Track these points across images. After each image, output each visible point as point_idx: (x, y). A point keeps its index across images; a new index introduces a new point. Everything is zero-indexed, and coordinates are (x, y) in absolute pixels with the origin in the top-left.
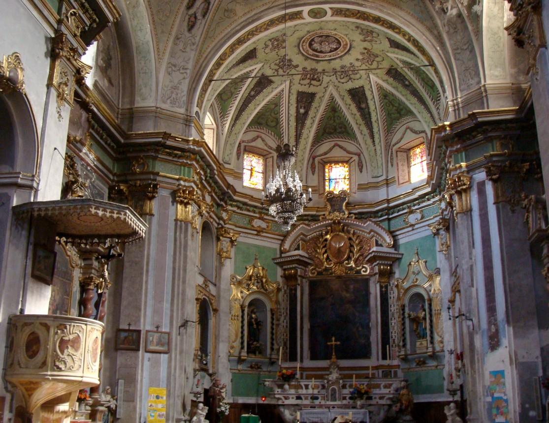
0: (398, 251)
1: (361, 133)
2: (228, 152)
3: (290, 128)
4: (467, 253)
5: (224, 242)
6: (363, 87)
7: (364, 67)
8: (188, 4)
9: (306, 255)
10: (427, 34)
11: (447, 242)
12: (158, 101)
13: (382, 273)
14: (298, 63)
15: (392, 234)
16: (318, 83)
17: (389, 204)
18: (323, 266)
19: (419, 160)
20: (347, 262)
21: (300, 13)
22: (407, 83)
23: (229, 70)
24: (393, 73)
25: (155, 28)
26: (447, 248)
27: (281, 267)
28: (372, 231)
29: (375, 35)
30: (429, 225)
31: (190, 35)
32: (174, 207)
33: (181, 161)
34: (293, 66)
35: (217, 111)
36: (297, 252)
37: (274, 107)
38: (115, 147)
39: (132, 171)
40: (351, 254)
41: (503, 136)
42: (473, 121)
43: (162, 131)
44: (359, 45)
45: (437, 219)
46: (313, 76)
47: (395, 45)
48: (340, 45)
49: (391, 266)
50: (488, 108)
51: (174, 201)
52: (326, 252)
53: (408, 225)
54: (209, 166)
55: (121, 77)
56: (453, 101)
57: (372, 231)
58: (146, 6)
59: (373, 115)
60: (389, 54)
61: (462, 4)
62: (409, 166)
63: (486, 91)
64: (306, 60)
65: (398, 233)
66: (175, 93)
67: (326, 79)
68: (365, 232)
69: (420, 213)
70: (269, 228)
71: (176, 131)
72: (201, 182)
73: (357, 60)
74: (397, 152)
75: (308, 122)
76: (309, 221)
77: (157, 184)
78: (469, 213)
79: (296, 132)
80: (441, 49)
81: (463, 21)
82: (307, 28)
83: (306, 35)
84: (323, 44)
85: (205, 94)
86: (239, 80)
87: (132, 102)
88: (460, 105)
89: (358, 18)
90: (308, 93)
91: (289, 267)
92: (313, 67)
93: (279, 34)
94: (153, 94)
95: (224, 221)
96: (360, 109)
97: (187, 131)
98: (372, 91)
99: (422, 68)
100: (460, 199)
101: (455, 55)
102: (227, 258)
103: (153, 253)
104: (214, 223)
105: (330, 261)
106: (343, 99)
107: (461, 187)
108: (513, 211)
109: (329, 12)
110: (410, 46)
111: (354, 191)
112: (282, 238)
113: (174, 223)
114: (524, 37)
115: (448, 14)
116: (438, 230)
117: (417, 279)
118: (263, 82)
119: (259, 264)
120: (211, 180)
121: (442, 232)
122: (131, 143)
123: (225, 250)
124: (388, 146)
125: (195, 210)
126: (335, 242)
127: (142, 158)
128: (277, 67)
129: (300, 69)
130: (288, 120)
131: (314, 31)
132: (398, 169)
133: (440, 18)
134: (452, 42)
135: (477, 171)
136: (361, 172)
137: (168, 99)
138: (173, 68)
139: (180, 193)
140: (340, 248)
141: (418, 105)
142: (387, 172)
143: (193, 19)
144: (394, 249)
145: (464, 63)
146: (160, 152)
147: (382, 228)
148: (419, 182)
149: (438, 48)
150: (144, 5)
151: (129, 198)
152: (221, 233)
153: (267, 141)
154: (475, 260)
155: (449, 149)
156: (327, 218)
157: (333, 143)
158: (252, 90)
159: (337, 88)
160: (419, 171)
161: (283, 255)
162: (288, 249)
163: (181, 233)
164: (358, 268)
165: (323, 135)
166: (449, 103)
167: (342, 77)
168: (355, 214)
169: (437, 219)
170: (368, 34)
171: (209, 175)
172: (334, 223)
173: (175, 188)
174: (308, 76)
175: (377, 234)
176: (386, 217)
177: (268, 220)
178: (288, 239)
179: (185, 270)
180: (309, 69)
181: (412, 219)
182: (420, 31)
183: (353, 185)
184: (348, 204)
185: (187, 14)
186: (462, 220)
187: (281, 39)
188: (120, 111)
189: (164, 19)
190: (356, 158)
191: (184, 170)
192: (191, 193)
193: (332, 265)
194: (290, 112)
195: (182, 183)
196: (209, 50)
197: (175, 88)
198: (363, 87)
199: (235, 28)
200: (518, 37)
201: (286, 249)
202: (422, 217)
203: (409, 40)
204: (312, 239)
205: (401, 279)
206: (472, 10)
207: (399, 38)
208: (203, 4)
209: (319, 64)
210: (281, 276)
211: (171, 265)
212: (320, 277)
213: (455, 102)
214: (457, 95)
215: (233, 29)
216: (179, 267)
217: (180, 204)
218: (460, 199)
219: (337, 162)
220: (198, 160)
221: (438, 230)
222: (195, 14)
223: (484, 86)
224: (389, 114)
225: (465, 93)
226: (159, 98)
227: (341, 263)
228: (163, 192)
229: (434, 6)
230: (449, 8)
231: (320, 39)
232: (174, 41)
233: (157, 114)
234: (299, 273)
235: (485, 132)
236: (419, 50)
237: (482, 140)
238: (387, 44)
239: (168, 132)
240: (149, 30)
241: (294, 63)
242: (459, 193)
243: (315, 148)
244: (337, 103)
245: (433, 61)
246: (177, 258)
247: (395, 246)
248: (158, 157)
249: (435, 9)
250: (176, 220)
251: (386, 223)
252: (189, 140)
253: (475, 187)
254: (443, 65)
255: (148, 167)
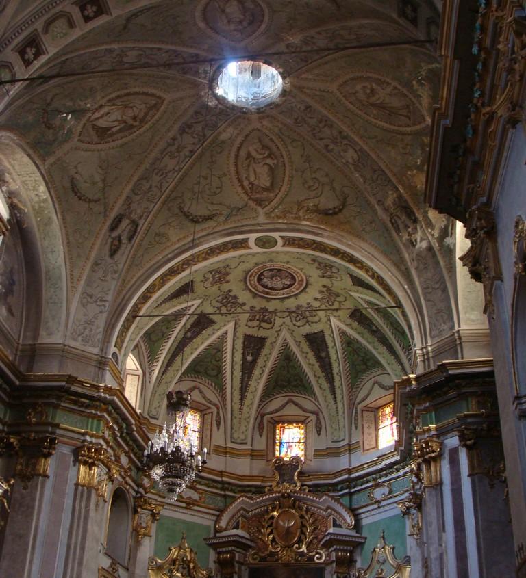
0: (361, 534)
1: (320, 388)
2: (156, 404)
3: (234, 379)
4: (436, 538)
5: (143, 516)
6: (322, 332)
7: (323, 307)
8: (112, 224)
9: (247, 536)
10: (394, 269)
11: (418, 524)
12: (68, 337)
13: (339, 562)
14: (245, 301)
15: (353, 511)
16: (268, 326)
17: (350, 474)
18: (267, 550)
19: (388, 422)
20: (297, 545)
21: (246, 241)
22: (374, 328)
23: (159, 306)
24: (357, 316)
25: (70, 251)
26: (419, 530)
27: (215, 549)
28: (328, 507)
29: (334, 270)
30: (397, 502)
31: (112, 261)
32: (75, 468)
33: (88, 411)
34: (239, 304)
35: (145, 354)
36: (235, 532)
37: (216, 351)
38: (8, 390)
39: (27, 419)
40: (303, 536)
41: (480, 393)
42: (442, 373)
43: (66, 373)
44: (317, 282)
45: (407, 494)
46: (263, 317)
47: (358, 282)
48: (295, 280)
49: (351, 552)
50: (462, 358)
51: (76, 461)
52: (271, 533)
53: (373, 502)
54: (125, 419)
55: (25, 305)
56: (422, 349)
57: (328, 507)
58: (60, 226)
59: (335, 365)
60: (352, 294)
61: (433, 235)
62: (377, 429)
63: (460, 338)
64: (254, 297)
65: (360, 511)
66: (88, 329)
67: (278, 321)
68: (321, 509)
69: (388, 487)
70: (203, 500)
71: (85, 375)
72: (115, 439)
73: (316, 299)
74: (362, 411)
75: (257, 372)
76: (254, 493)
77: (55, 439)
78: (439, 487)
79: (242, 383)
80: (409, 288)
81: (434, 256)
82: (255, 260)
83: (254, 267)
84: (274, 279)
85: (126, 332)
86: (173, 317)
87: (36, 336)
88: (431, 355)
89: (314, 250)
90: (257, 337)
91: (224, 549)
92: (263, 307)
93: (222, 265)
94: (62, 328)
95: (145, 489)
96: (319, 358)
97: (100, 376)
98: (333, 337)
99: (388, 309)
100: (429, 469)
101: (425, 295)
102: (145, 535)
103: (43, 524)
104: (131, 490)
105: (277, 544)
106: (299, 346)
107: (429, 455)
108: (492, 486)
109: (280, 242)
110: (374, 283)
111: (309, 457)
112: (217, 513)
113: (73, 487)
114: (480, 268)
115: (417, 247)
116: (408, 508)
117: (382, 570)
118: (202, 322)
119: (186, 545)
120: (128, 436)
121: (413, 511)
122: (31, 387)
123: (144, 525)
124: (352, 404)
125: (102, 473)
126: (283, 521)
127: (40, 406)
128: (219, 305)
129: (247, 308)
130: (232, 368)
131: (263, 263)
132: (363, 433)
133: (407, 252)
134: (422, 279)
135: (449, 435)
136: (319, 434)
137: (79, 335)
138: (89, 299)
139: (84, 451)
140: (289, 527)
141: (387, 354)
142: (350, 435)
143: (116, 242)
144: (355, 531)
145: (435, 305)
146: (64, 399)
147: (341, 504)
148: (387, 448)
149: (406, 287)
150: (57, 223)
151: (20, 453)
152: (140, 502)
153: (205, 393)
154: (446, 547)
155: (416, 408)
156: (275, 489)
157: (287, 399)
158: (189, 330)
159: (292, 332)
160: (387, 435)
161: (218, 535)
162: (224, 527)
163: (81, 501)
164: (311, 554)
165: (274, 388)
166: (418, 352)
167: (298, 319)
168: (309, 486)
169: (407, 494)
170: (326, 268)
171: (125, 431)
172: (283, 496)
173: (79, 444)
174: (257, 317)
175: (336, 511)
176: (347, 491)
177: (200, 489)
178: (222, 518)
179: (83, 548)
180: (258, 308)
181: (378, 493)
182: (385, 266)
183: (308, 449)
184: (301, 474)
185: (109, 236)
186: (430, 495)
187: (223, 270)
188: (20, 347)
189: (80, 241)
190: (313, 417)
191: (92, 423)
192: (98, 451)
193: (279, 549)
194: (235, 359)
195: (88, 438)
196: (134, 280)
197: (90, 323)
198: (322, 332)
199: (167, 255)
200: (474, 268)
201: (221, 527)
202: (390, 492)
203: (372, 277)
204: (255, 516)
205: (363, 570)
206: (444, 243)
207: (361, 274)
208: (130, 226)
209: (270, 303)
210: (215, 562)
211: (66, 541)
212: (263, 564)
213: (424, 350)
214: (426, 342)
215: (165, 257)
216: (76, 543)
217: (84, 465)
218: (429, 469)
219: (290, 422)
220: (111, 411)
221: (408, 508)
222: (119, 237)
223: (458, 331)
224: (353, 365)
225: (437, 340)
226: (69, 334)
227: (290, 547)
228: (63, 448)
229: (401, 237)
230: (418, 240)
231: (271, 273)
232: (92, 266)
233: (64, 353)
234: (237, 558)
235: (458, 387)
236: (384, 289)
237: (455, 398)
238: (350, 282)
239: (75, 375)
240: (62, 253)
241: (240, 301)
242: (427, 462)
243: (264, 403)
244: (292, 350)
245: (400, 302)
246: (74, 533)
247: (357, 527)
248: (60, 405)
249: (402, 241)
250: (77, 484)
251: (347, 498)
252: (99, 387)
253: (446, 455)
254: (412, 308)
255: (47, 416)
